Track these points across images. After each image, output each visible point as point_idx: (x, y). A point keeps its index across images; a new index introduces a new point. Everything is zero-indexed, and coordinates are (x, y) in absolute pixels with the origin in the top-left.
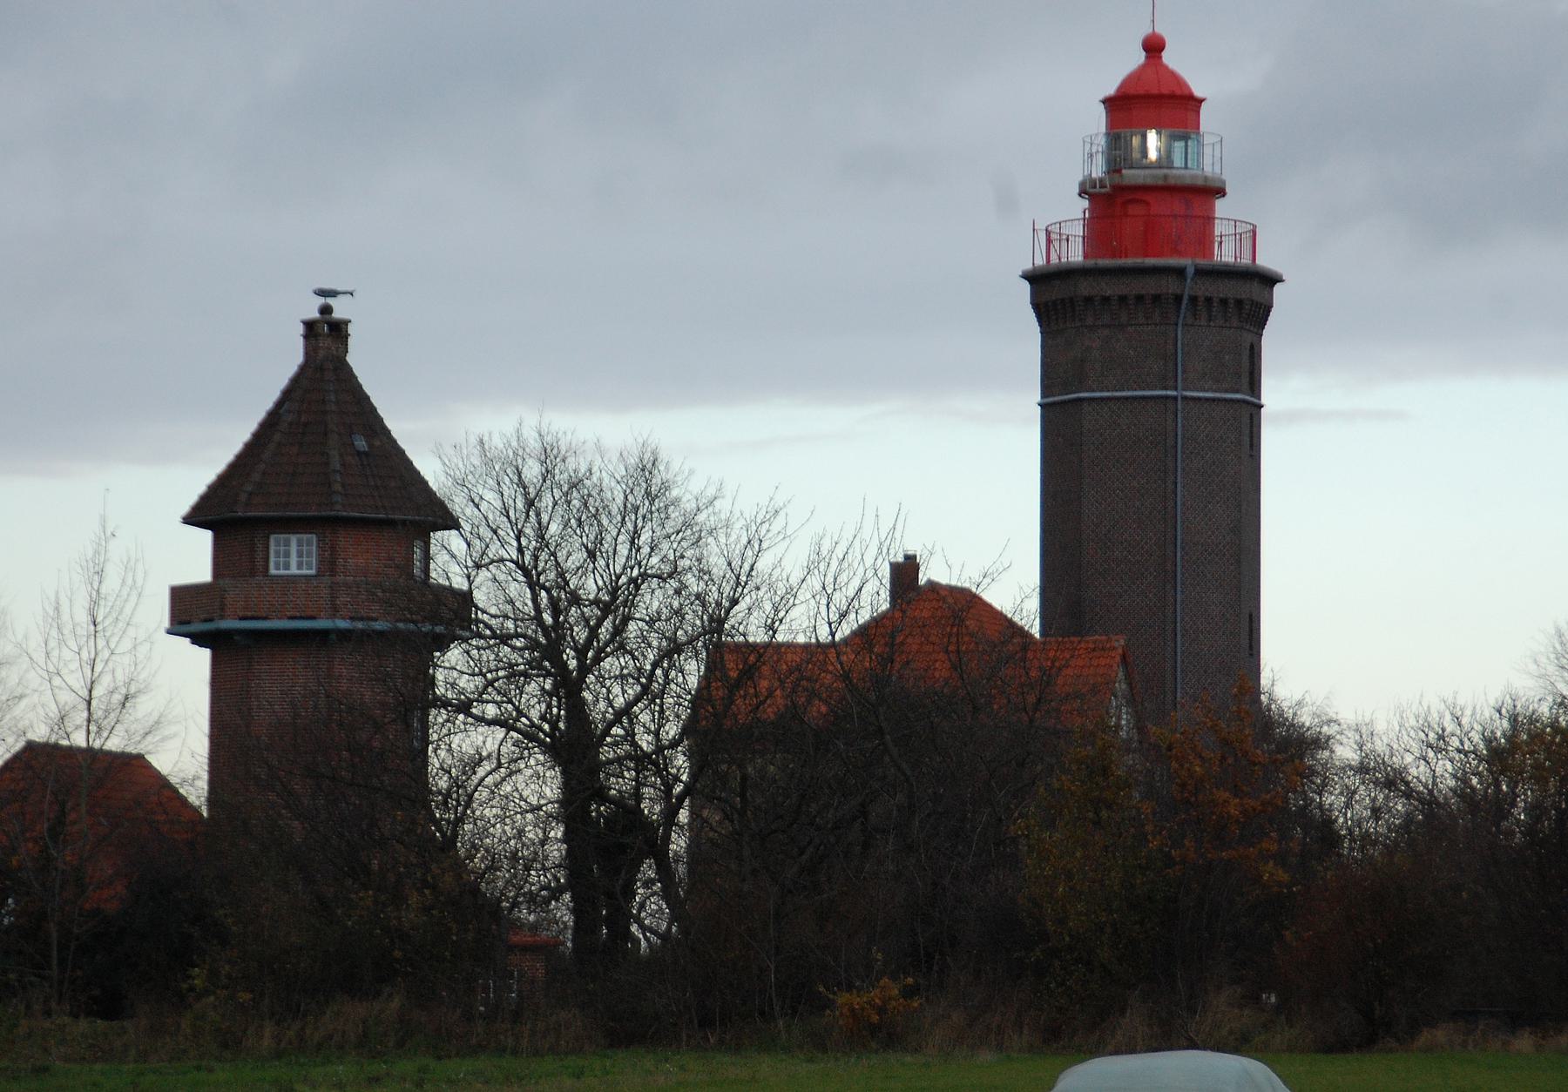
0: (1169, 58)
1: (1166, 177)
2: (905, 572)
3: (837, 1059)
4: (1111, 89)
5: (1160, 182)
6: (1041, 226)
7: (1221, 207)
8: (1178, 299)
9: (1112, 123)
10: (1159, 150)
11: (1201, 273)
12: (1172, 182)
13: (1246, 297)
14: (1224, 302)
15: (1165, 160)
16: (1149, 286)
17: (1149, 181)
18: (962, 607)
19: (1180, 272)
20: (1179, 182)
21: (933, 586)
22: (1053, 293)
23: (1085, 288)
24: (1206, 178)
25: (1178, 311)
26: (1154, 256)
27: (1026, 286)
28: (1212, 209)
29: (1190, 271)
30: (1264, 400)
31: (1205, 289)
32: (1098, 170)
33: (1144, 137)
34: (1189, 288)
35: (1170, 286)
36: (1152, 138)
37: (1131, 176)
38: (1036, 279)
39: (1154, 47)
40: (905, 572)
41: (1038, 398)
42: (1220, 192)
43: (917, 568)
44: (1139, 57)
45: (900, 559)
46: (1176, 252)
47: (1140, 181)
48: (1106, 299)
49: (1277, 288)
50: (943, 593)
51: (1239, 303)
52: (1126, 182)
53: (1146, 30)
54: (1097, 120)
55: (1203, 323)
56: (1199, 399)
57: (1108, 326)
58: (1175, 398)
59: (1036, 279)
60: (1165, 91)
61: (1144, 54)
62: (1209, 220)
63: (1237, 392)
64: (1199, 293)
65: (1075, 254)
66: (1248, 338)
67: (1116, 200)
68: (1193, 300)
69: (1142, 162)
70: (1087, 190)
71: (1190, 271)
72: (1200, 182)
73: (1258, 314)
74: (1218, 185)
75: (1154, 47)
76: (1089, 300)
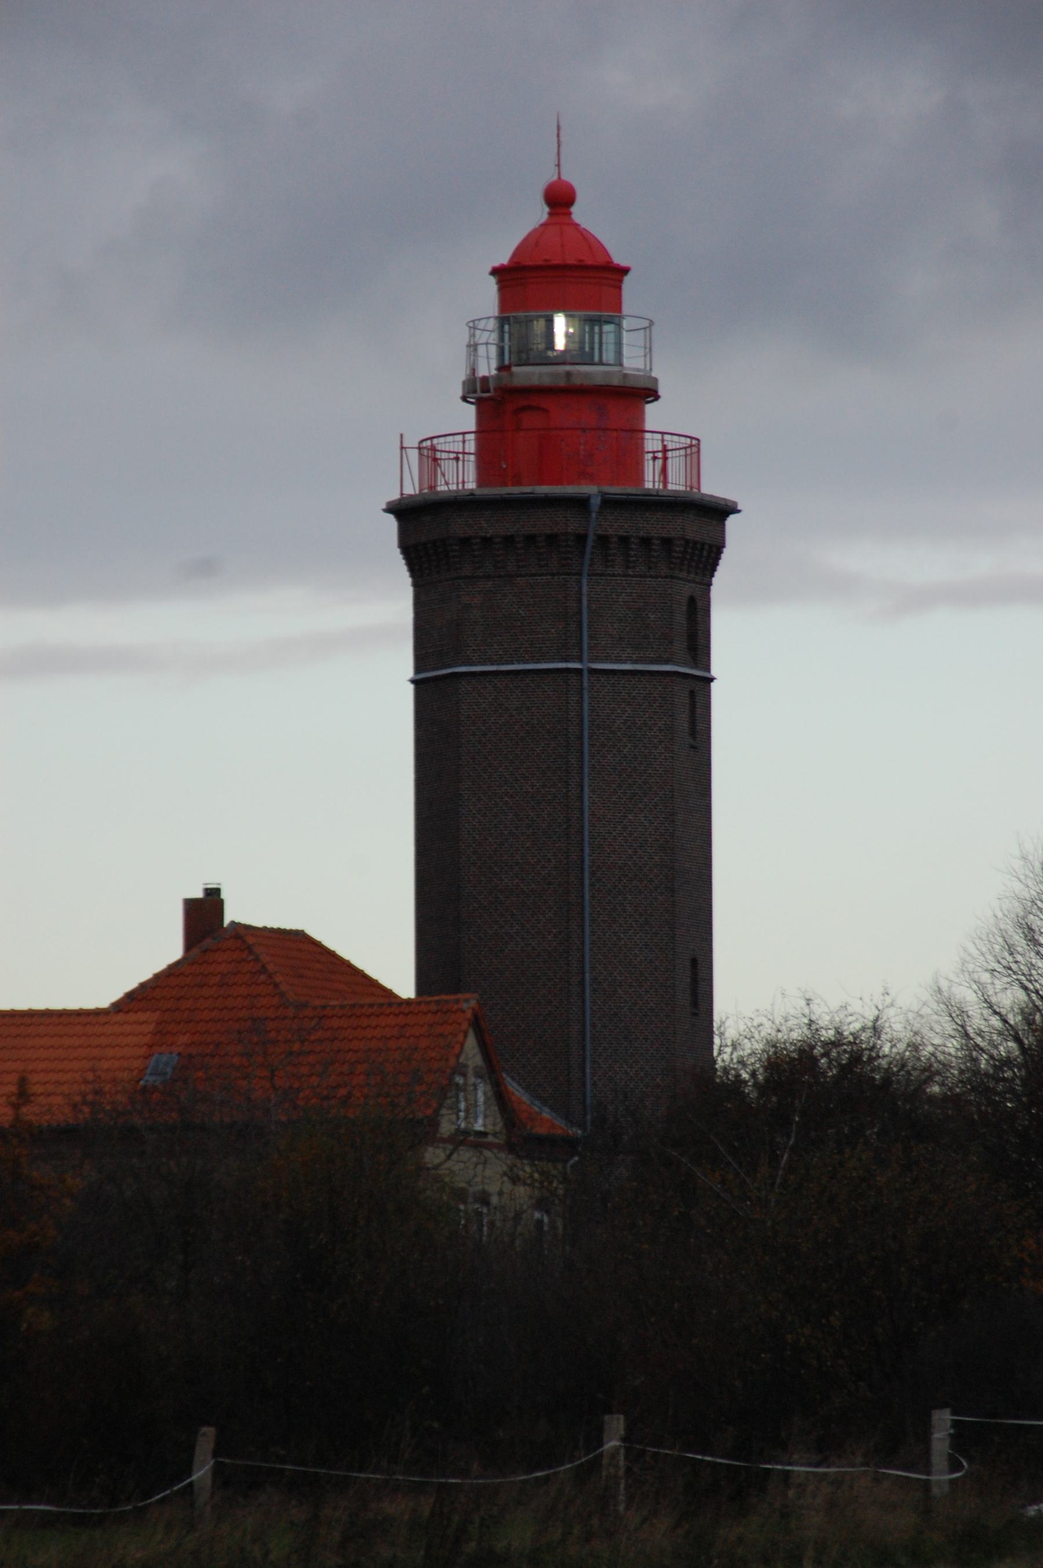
0: (579, 213)
1: (568, 374)
2: (203, 913)
3: (914, 1047)
4: (503, 258)
5: (562, 383)
6: (412, 441)
7: (654, 416)
8: (582, 538)
9: (506, 302)
10: (567, 335)
11: (610, 503)
12: (577, 381)
13: (688, 537)
14: (646, 541)
15: (582, 351)
16: (541, 523)
17: (547, 381)
18: (298, 955)
19: (581, 503)
20: (587, 382)
21: (241, 931)
22: (429, 533)
23: (460, 526)
24: (625, 376)
25: (582, 553)
26: (551, 483)
27: (391, 523)
28: (641, 417)
29: (596, 502)
30: (715, 671)
31: (616, 525)
32: (487, 368)
33: (550, 322)
34: (595, 525)
35: (569, 523)
36: (560, 324)
37: (527, 375)
38: (404, 511)
39: (560, 199)
40: (203, 913)
41: (409, 671)
42: (651, 394)
43: (220, 903)
44: (539, 213)
45: (199, 894)
46: (584, 476)
47: (535, 381)
48: (487, 541)
49: (731, 521)
50: (250, 940)
51: (667, 542)
52: (517, 382)
53: (549, 176)
54: (487, 297)
55: (618, 570)
56: (613, 672)
57: (488, 577)
58: (579, 672)
59: (404, 511)
60: (571, 261)
61: (547, 209)
62: (637, 431)
63: (667, 662)
64: (610, 532)
65: (461, 477)
66: (685, 590)
67: (502, 404)
68: (603, 540)
69: (546, 356)
70: (475, 390)
71: (596, 502)
72: (616, 382)
73: (708, 555)
74: (643, 384)
75: (560, 199)
76: (465, 541)
